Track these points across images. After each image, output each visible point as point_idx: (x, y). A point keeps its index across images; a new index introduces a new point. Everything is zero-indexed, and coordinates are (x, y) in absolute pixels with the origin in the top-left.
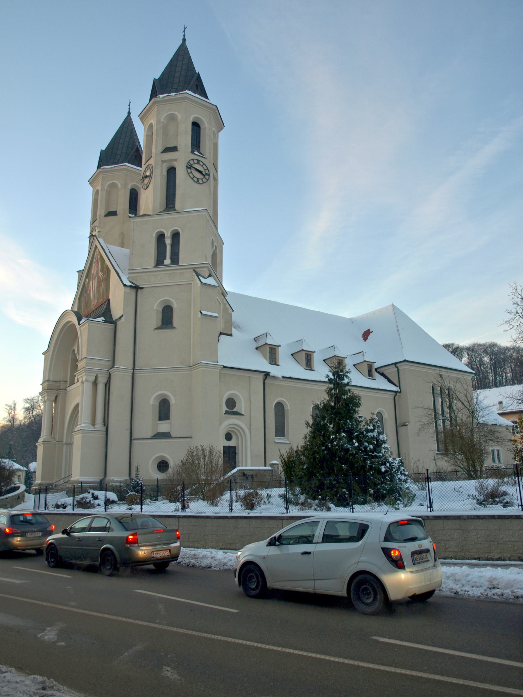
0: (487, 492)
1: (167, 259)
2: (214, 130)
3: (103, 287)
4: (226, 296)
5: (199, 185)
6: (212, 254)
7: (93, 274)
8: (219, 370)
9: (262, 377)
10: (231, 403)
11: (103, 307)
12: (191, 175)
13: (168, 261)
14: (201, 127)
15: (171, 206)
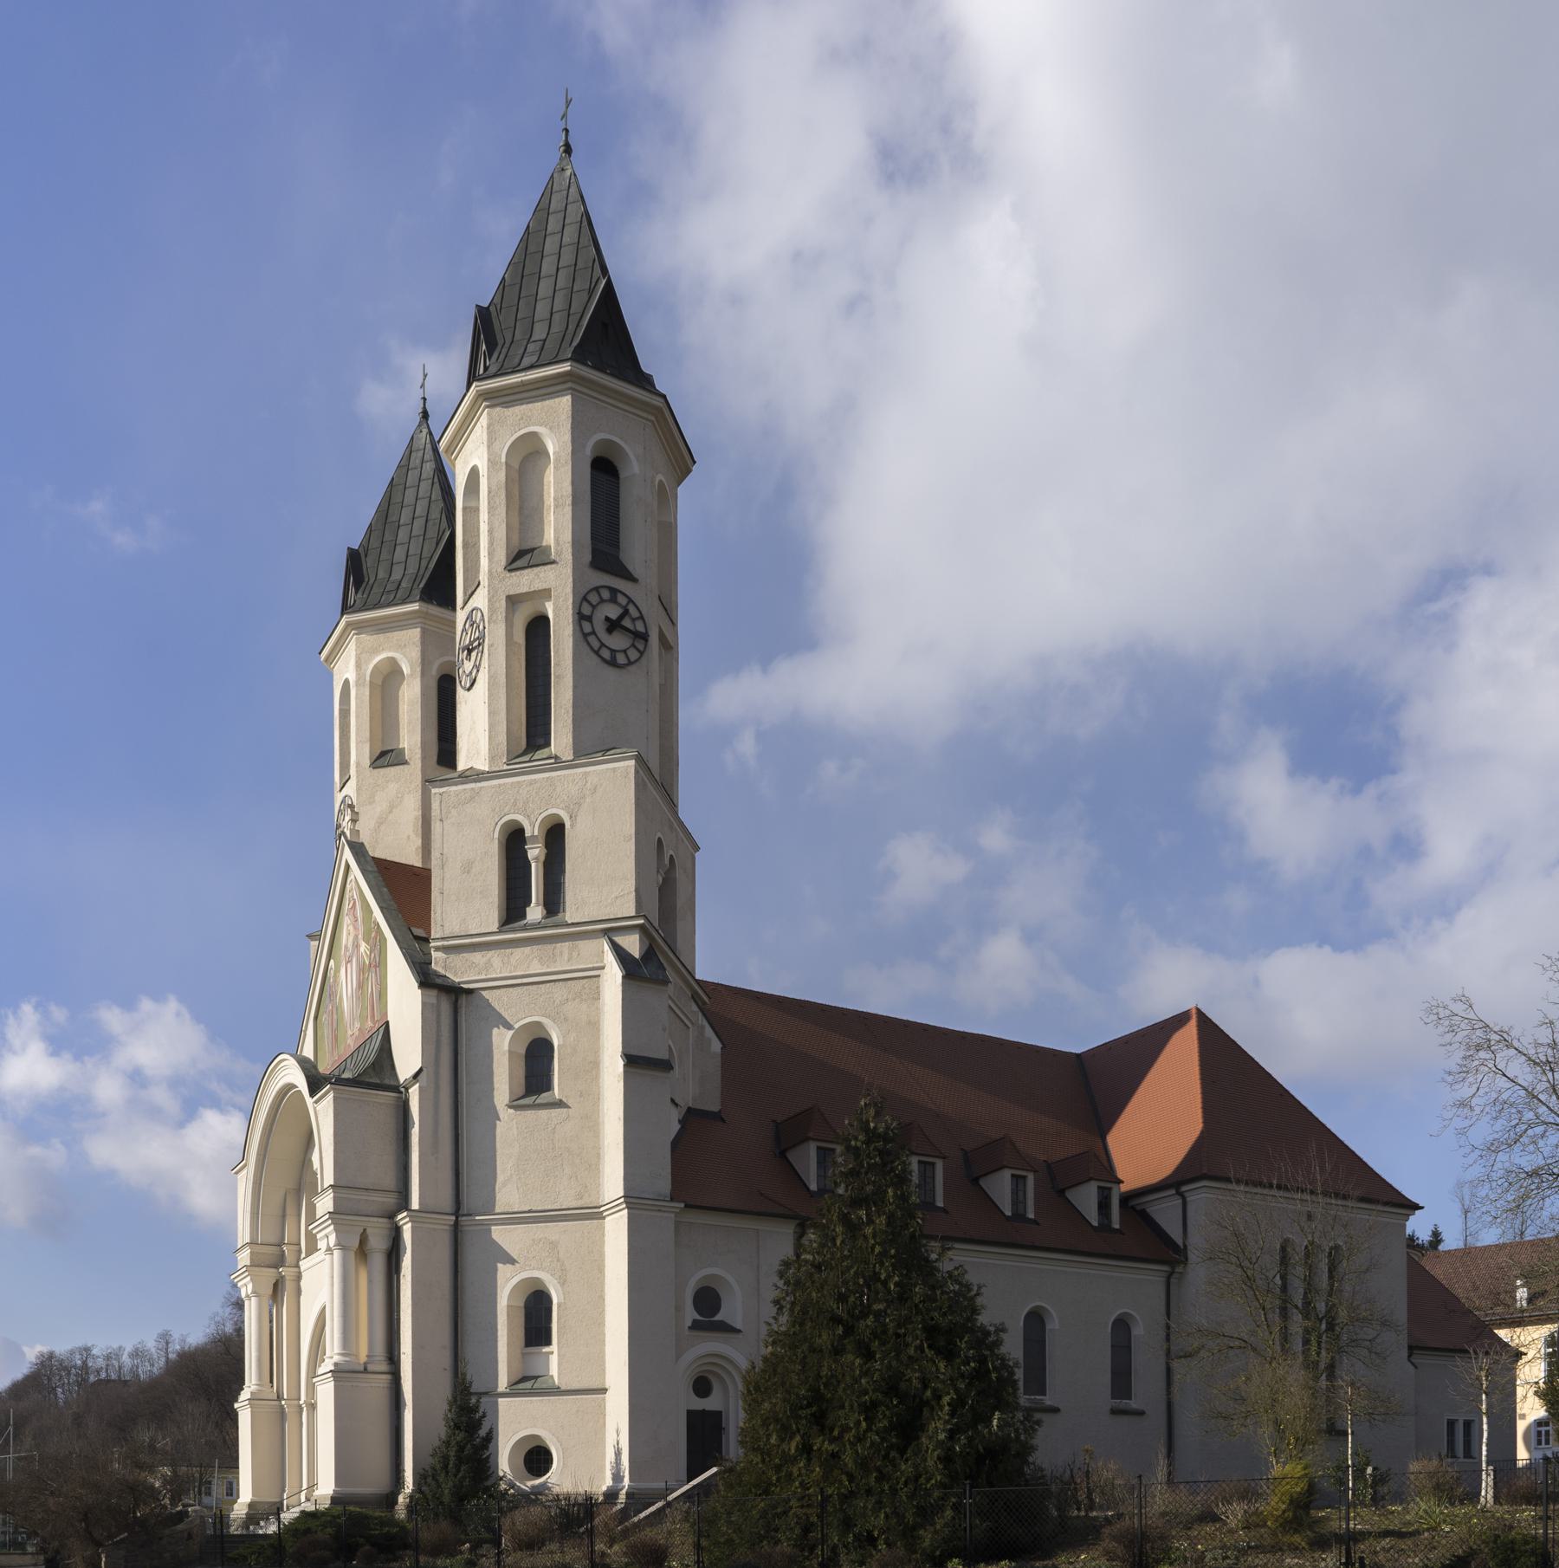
1: (532, 905)
2: (661, 481)
3: (371, 986)
5: (617, 670)
7: (346, 947)
8: (673, 1215)
9: (792, 1231)
10: (707, 1300)
11: (373, 1043)
12: (592, 639)
13: (535, 912)
14: (622, 475)
15: (541, 741)
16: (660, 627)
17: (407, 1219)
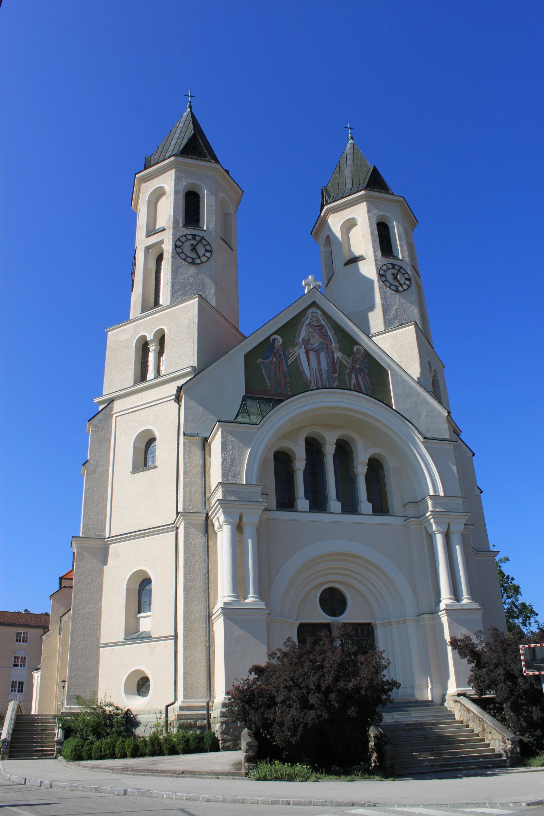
0: (314, 684)
4: (460, 435)
6: (432, 381)
12: (387, 283)
16: (415, 279)
17: (429, 499)
